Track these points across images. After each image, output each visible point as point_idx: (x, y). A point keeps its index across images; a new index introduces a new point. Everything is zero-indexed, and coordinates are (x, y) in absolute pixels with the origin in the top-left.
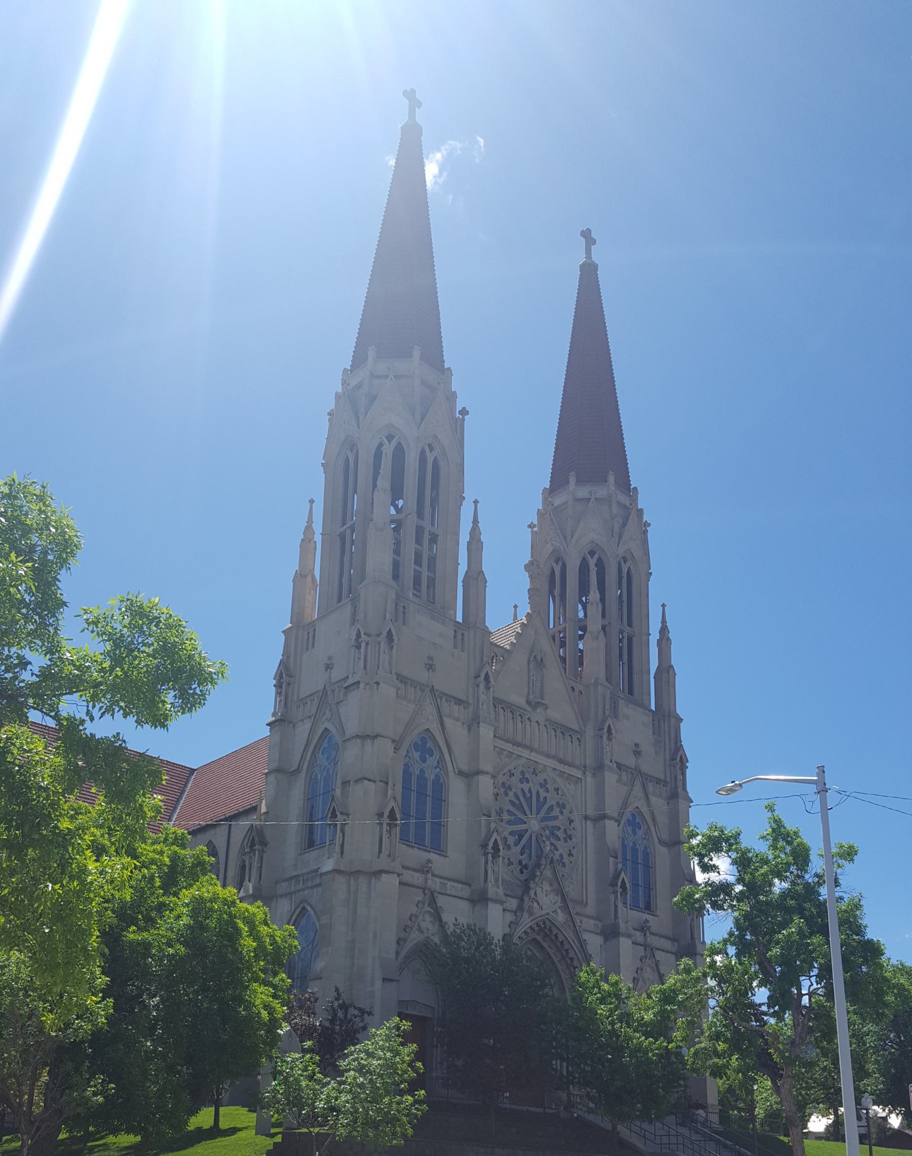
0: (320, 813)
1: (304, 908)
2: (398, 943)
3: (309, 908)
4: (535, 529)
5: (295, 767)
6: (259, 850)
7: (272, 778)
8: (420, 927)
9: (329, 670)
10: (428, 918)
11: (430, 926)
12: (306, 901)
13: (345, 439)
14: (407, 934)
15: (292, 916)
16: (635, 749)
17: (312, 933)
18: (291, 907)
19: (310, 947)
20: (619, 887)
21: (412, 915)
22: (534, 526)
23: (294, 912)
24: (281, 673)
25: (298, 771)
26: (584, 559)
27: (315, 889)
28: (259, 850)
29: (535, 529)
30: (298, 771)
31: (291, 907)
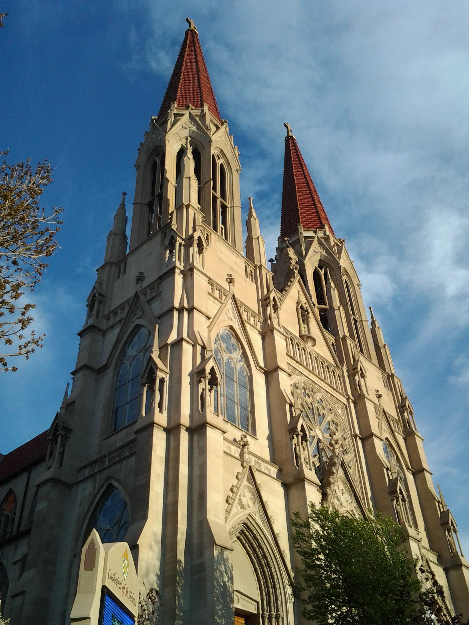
0: (126, 420)
1: (111, 486)
2: (227, 501)
3: (116, 484)
4: (275, 262)
5: (104, 363)
6: (62, 435)
7: (80, 375)
8: (242, 502)
9: (140, 282)
10: (247, 494)
11: (251, 504)
12: (112, 477)
13: (154, 150)
14: (230, 506)
15: (95, 497)
16: (376, 393)
17: (118, 512)
18: (94, 489)
19: (116, 529)
20: (399, 494)
21: (233, 486)
22: (273, 261)
23: (98, 493)
24: (94, 296)
25: (105, 368)
26: (316, 269)
27: (125, 462)
28: (62, 435)
29: (275, 262)
30: (105, 368)
31: (94, 489)
